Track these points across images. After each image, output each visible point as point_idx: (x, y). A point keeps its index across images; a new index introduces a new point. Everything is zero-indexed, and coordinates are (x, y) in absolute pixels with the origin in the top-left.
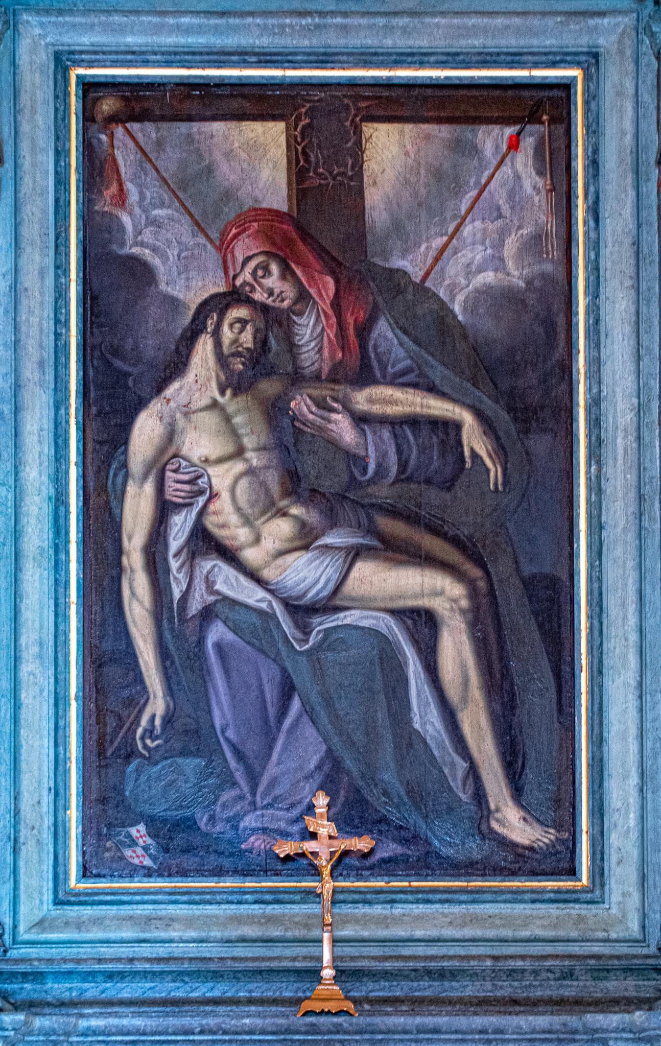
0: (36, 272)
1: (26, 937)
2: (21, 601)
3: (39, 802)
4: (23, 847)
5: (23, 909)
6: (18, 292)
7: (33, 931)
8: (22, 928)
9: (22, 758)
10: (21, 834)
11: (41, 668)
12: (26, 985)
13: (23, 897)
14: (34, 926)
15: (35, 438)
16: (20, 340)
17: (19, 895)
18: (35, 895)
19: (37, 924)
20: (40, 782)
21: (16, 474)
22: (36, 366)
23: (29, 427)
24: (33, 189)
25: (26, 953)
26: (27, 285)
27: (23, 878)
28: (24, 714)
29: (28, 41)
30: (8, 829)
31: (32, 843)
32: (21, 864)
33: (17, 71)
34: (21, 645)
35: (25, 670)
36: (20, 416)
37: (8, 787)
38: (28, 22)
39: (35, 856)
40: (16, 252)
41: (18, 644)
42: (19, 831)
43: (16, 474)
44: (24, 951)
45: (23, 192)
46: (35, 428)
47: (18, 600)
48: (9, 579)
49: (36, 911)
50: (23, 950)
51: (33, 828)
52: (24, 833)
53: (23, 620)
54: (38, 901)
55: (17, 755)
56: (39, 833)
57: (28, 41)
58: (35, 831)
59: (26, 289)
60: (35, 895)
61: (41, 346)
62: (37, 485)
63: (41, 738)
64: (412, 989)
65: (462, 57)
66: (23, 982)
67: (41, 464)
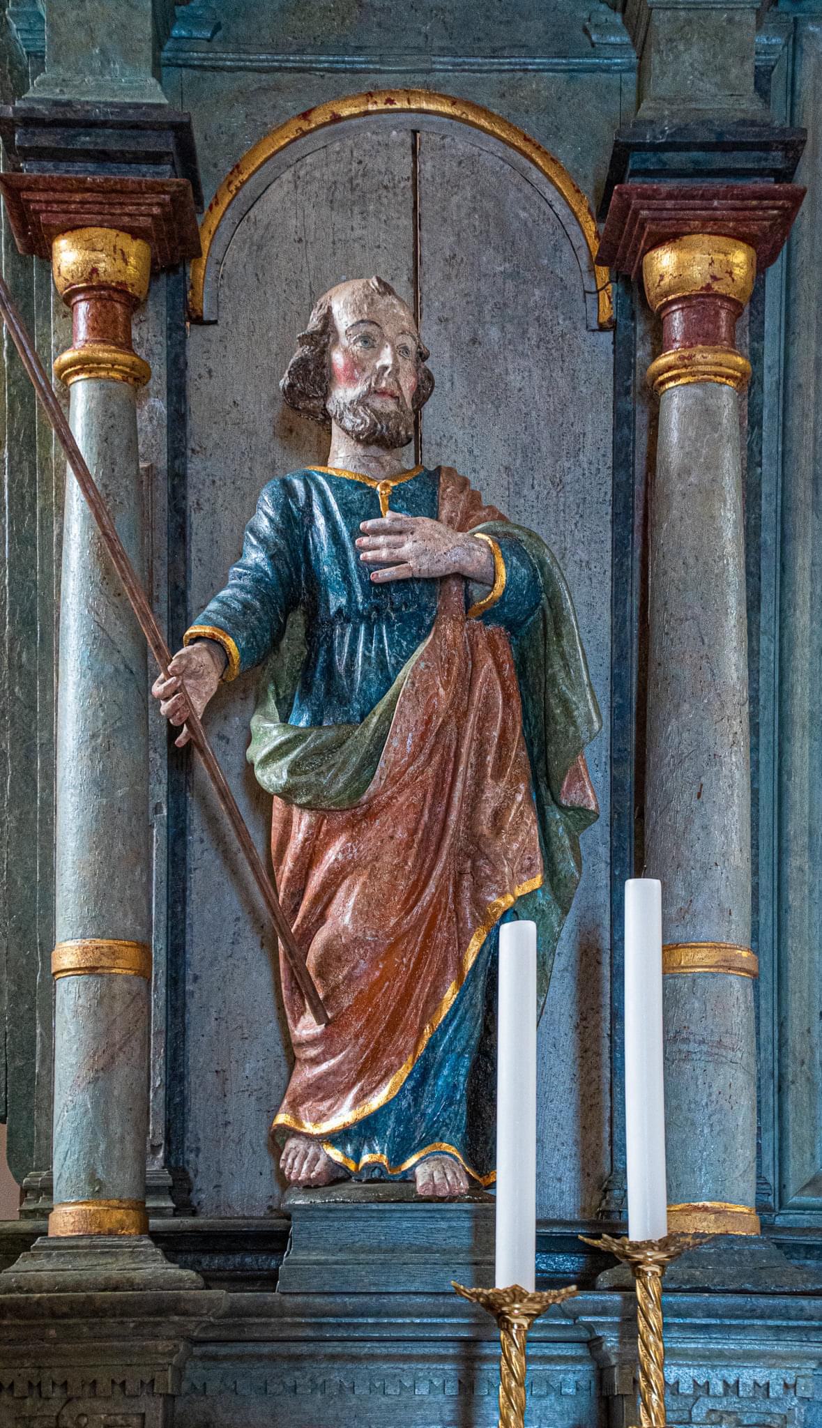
0: (812, 364)
1: (794, 1200)
2: (789, 779)
3: (809, 1031)
4: (792, 1087)
5: (793, 1166)
6: (790, 390)
7: (806, 1193)
8: (791, 1188)
9: (791, 974)
10: (790, 1069)
11: (811, 864)
12: (808, 1262)
13: (792, 1149)
14: (805, 1186)
15: (807, 574)
16: (790, 451)
17: (787, 1146)
18: (807, 1148)
19: (808, 1185)
20: (810, 1006)
21: (782, 621)
22: (809, 484)
23: (800, 561)
24: (812, 256)
25: (796, 1220)
26: (802, 380)
27: (791, 1125)
28: (793, 920)
29: (813, 60)
30: (770, 1063)
31: (801, 1081)
32: (789, 1107)
33: (797, 101)
34: (788, 834)
35: (793, 865)
36: (789, 548)
37: (770, 1011)
38: (814, 35)
39: (806, 1099)
40: (786, 338)
41: (784, 832)
42: (787, 1066)
43: (782, 621)
44: (792, 1218)
45: (799, 261)
46: (808, 562)
47: (785, 777)
48: (771, 751)
49: (807, 1168)
50: (791, 1217)
51: (803, 1063)
52: (792, 1069)
53: (791, 802)
54: (808, 1155)
55: (784, 970)
56: (809, 1068)
57: (813, 60)
58: (805, 1067)
59: (800, 386)
60: (807, 1148)
61: (814, 459)
62: (807, 633)
63: (811, 949)
64: (157, 964)
65: (99, 971)
66: (806, 1258)
67: (812, 607)
